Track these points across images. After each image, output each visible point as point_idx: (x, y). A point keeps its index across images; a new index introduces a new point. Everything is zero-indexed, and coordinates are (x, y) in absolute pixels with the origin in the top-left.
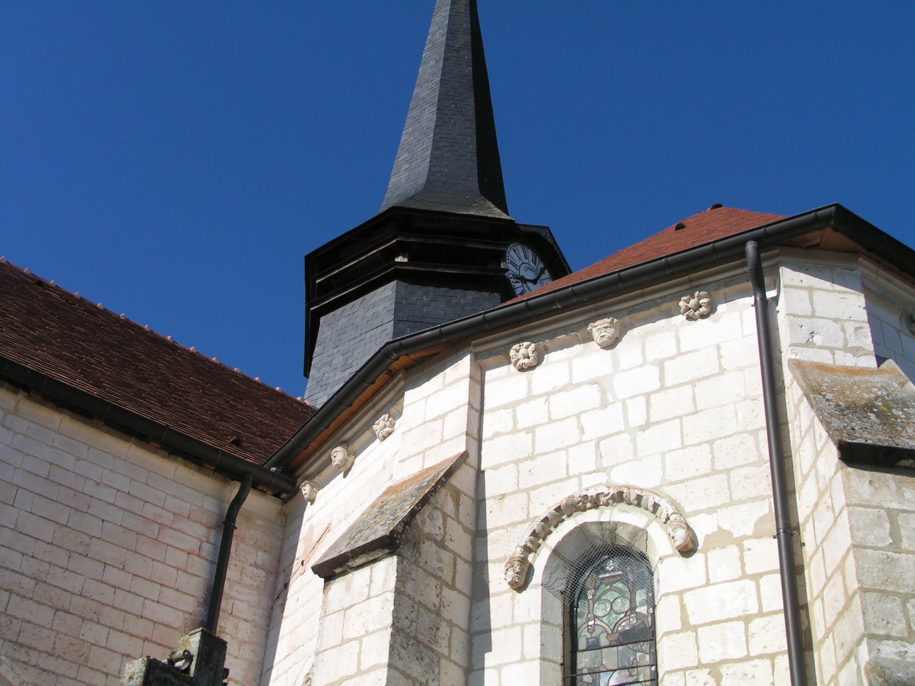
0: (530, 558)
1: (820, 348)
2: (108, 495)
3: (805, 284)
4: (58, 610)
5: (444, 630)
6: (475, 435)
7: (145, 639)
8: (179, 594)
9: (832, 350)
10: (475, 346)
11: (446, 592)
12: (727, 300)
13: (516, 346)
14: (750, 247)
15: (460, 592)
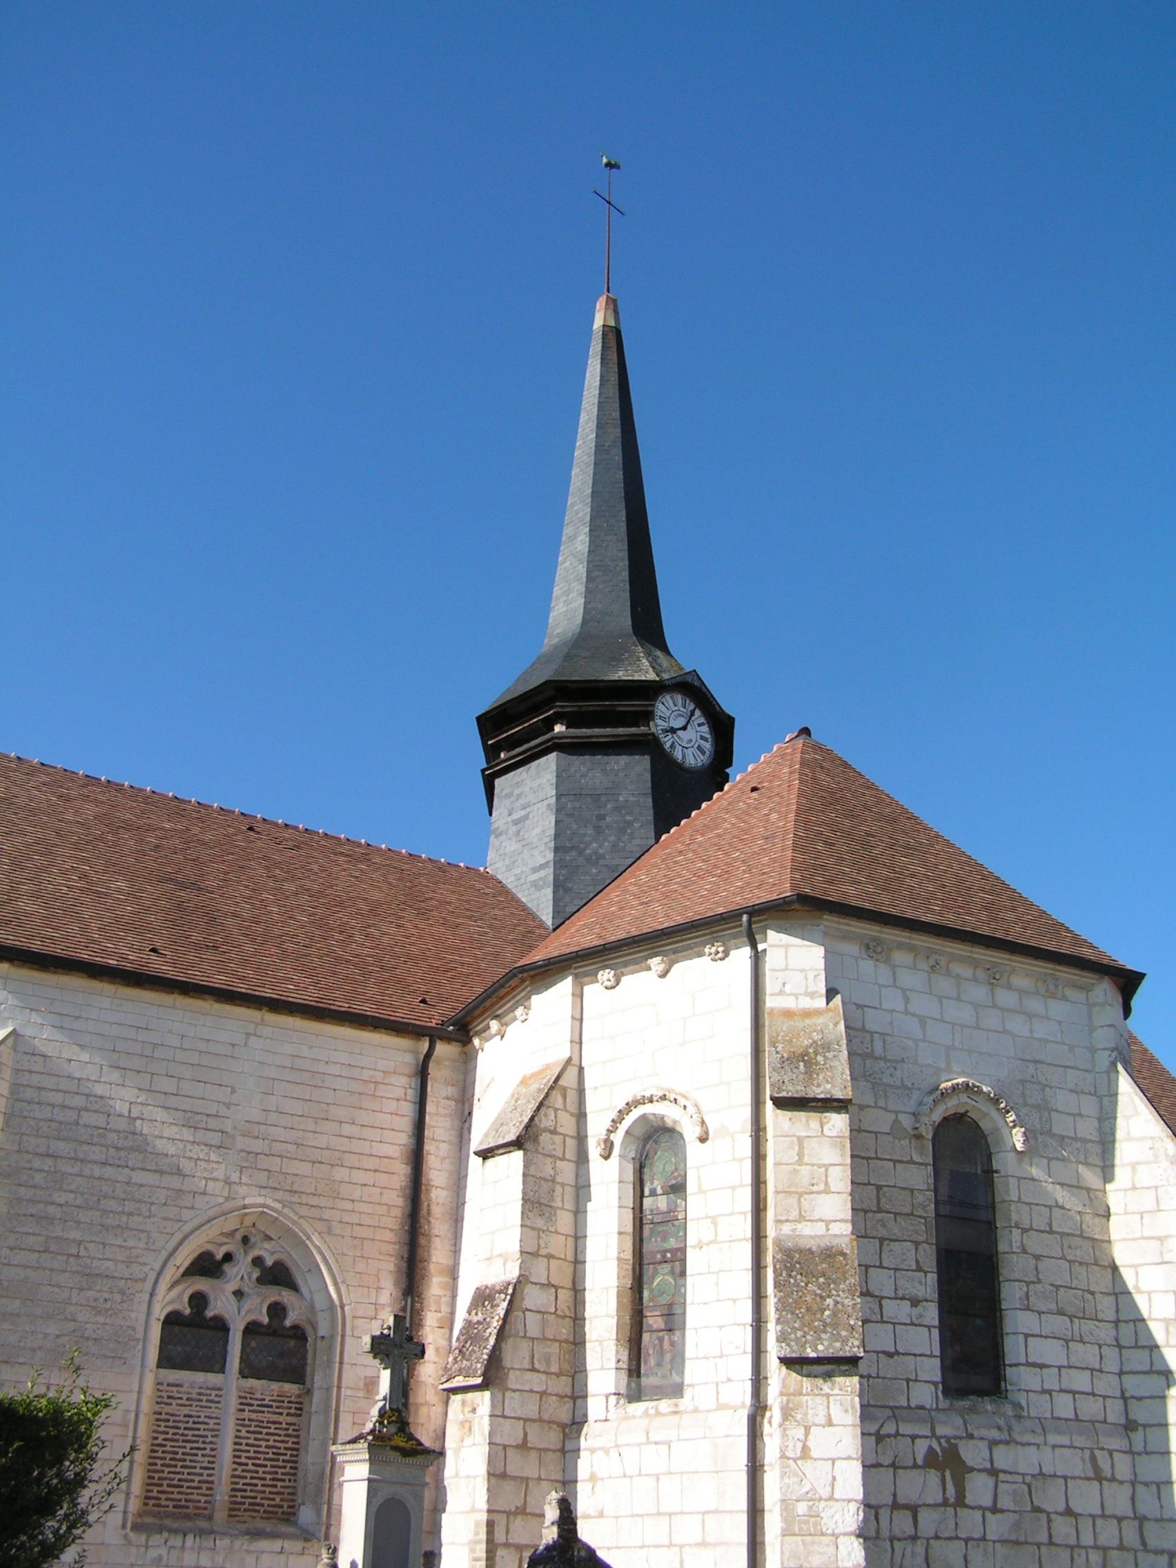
0: (612, 1136)
1: (788, 995)
2: (335, 1070)
3: (783, 942)
4: (314, 1162)
5: (559, 1189)
6: (578, 1042)
7: (375, 1171)
8: (394, 1133)
9: (796, 996)
10: (575, 968)
11: (559, 1163)
13: (601, 972)
14: (745, 918)
15: (568, 1160)
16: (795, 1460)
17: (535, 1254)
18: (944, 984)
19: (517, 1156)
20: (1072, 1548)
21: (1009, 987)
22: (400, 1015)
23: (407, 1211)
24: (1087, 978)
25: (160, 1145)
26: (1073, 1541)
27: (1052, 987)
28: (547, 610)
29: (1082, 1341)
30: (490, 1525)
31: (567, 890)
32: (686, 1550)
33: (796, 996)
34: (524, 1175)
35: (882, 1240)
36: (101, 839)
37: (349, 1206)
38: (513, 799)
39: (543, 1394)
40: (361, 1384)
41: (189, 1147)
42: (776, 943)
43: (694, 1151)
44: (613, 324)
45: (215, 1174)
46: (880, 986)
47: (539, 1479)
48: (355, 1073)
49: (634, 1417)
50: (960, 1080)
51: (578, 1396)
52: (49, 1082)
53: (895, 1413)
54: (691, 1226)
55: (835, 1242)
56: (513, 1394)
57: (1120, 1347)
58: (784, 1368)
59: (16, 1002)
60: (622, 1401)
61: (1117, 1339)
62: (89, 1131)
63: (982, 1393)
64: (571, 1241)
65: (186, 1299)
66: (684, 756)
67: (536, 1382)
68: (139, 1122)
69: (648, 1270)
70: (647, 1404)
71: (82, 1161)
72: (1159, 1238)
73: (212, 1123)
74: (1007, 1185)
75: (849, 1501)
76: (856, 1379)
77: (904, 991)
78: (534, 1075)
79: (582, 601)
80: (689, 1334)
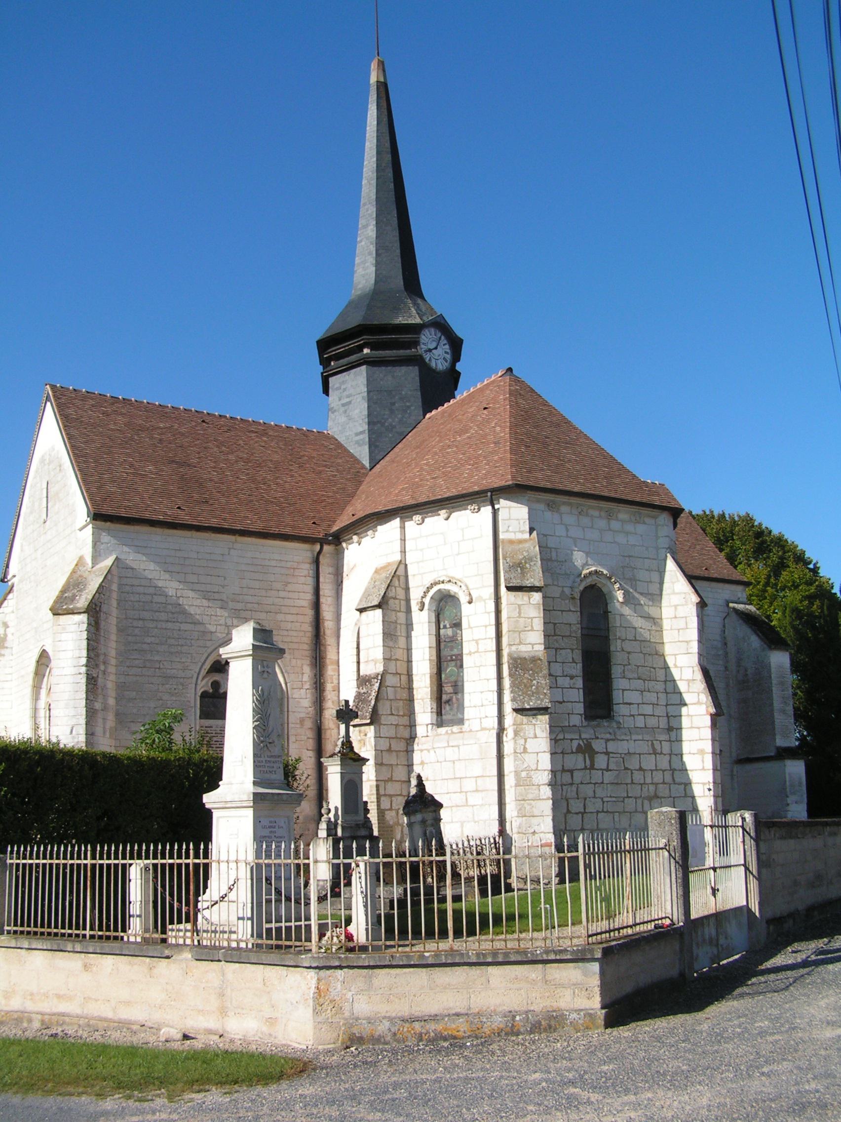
2: (273, 563)
5: (399, 626)
6: (403, 552)
7: (297, 614)
9: (515, 532)
12: (484, 506)
14: (489, 494)
16: (520, 753)
17: (390, 659)
18: (585, 521)
19: (379, 612)
20: (641, 784)
21: (617, 519)
22: (304, 532)
23: (314, 633)
24: (656, 512)
25: (192, 610)
26: (642, 782)
27: (638, 518)
28: (352, 273)
29: (649, 691)
30: (377, 786)
31: (377, 447)
32: (469, 794)
33: (515, 532)
34: (383, 621)
35: (556, 649)
36: (132, 439)
37: (286, 633)
38: (341, 391)
39: (397, 725)
40: (298, 722)
41: (207, 609)
42: (503, 504)
43: (466, 609)
44: (382, 80)
45: (221, 622)
46: (555, 524)
47: (397, 764)
48: (283, 564)
49: (441, 735)
50: (593, 569)
51: (412, 725)
52: (136, 582)
53: (563, 729)
54: (464, 644)
55: (537, 654)
56: (384, 727)
57: (667, 693)
58: (515, 713)
59: (116, 541)
60: (434, 727)
61: (665, 689)
62: (158, 605)
63: (602, 717)
64: (405, 651)
65: (210, 684)
66: (436, 364)
67: (393, 720)
68: (181, 599)
69: (444, 665)
70: (447, 728)
71: (156, 621)
72: (687, 642)
73: (216, 596)
74: (615, 618)
75: (545, 770)
76: (547, 717)
77: (566, 525)
78: (382, 568)
79: (374, 269)
80: (466, 697)
